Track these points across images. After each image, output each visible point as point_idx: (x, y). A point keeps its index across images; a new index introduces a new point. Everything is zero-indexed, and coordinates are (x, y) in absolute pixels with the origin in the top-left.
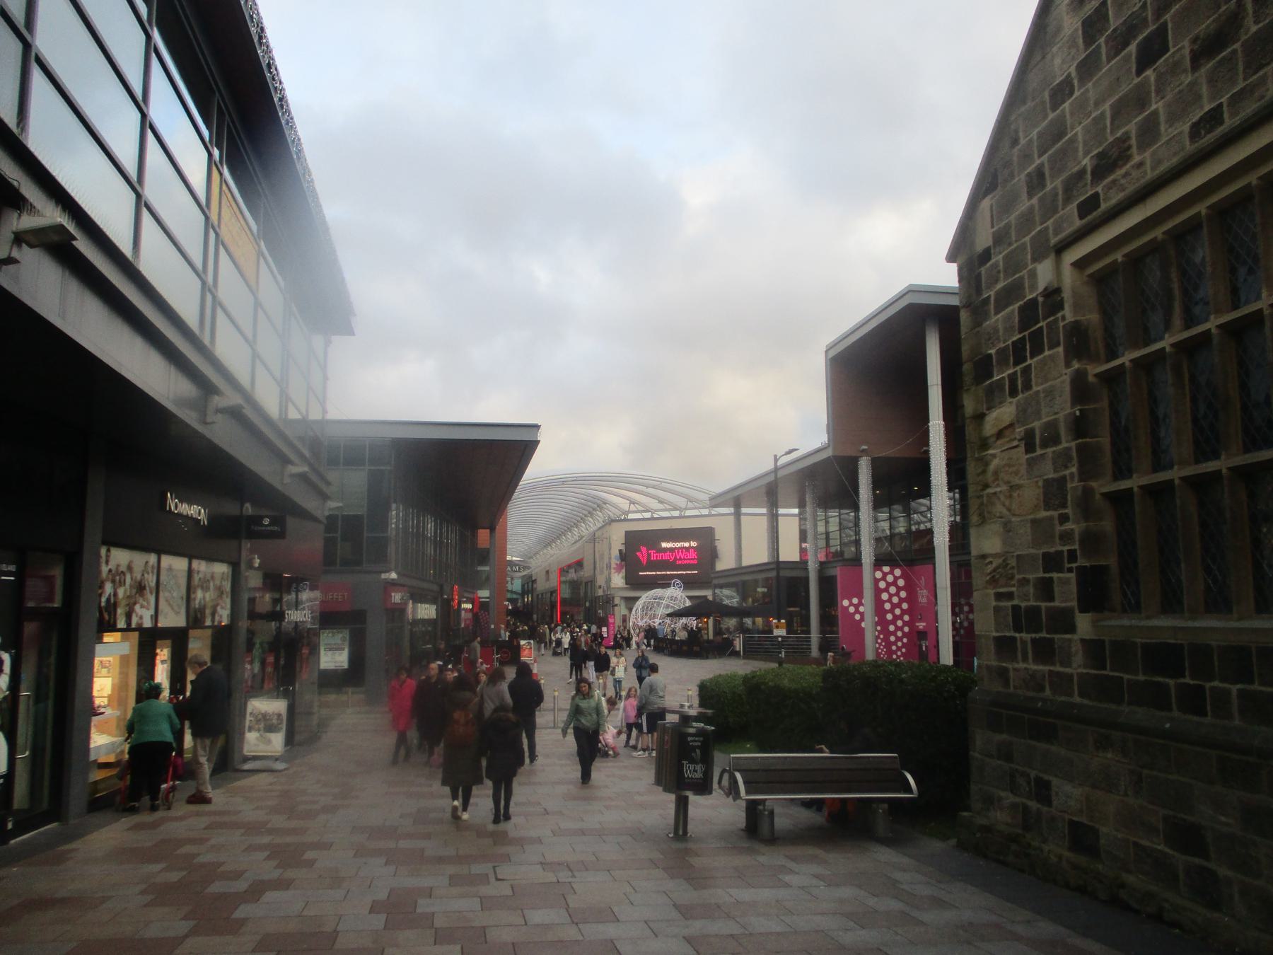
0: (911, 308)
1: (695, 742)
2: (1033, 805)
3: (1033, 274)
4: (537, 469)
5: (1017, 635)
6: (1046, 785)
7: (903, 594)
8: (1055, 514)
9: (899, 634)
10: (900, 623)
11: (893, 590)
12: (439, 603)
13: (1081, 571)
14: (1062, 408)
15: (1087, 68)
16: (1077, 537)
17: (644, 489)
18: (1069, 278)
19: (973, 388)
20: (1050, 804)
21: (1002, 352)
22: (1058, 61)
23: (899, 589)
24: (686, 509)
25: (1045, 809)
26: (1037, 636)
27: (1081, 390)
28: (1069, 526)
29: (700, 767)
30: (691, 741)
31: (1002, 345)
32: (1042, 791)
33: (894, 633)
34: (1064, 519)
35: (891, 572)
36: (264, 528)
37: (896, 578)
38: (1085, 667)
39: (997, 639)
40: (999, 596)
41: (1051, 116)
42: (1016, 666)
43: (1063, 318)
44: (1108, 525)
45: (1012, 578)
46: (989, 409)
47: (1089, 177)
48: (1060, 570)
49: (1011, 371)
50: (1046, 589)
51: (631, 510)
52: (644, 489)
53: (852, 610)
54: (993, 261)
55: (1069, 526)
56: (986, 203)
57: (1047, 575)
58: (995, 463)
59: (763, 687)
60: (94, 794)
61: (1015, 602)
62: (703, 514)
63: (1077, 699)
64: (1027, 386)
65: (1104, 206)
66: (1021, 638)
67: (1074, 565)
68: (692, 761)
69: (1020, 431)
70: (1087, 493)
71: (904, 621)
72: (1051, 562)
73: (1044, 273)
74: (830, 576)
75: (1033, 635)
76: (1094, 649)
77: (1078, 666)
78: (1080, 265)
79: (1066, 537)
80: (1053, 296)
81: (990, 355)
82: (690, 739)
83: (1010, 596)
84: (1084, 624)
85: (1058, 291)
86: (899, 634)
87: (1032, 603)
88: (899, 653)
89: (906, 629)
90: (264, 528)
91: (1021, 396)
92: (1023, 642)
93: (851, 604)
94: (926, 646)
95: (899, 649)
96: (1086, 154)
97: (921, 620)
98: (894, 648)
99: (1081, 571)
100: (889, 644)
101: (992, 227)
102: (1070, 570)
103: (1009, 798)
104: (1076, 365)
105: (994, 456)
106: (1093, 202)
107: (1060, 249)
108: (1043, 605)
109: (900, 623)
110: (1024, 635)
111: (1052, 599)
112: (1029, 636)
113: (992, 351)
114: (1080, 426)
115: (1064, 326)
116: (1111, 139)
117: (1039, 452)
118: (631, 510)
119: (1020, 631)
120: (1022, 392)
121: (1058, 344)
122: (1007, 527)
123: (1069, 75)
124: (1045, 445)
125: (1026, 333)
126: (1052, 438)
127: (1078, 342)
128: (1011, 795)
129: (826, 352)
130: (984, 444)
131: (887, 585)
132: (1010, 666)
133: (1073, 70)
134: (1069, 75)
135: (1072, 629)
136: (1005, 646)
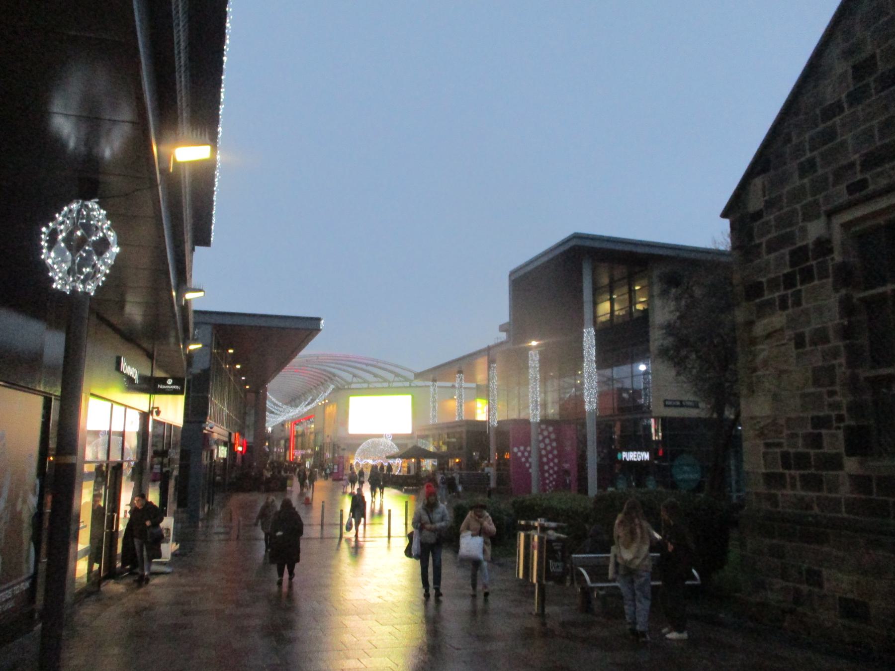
0: (573, 249)
1: (557, 546)
2: (805, 588)
3: (804, 230)
4: (312, 349)
5: (787, 472)
6: (819, 574)
7: (554, 444)
8: (824, 390)
9: (551, 472)
10: (551, 464)
11: (547, 441)
12: (228, 446)
13: (848, 428)
14: (833, 318)
15: (855, 98)
16: (845, 406)
17: (364, 367)
18: (837, 236)
19: (744, 304)
20: (821, 586)
21: (770, 281)
22: (829, 89)
23: (551, 441)
24: (393, 381)
25: (816, 590)
26: (806, 472)
27: (847, 308)
28: (837, 398)
29: (560, 564)
30: (555, 546)
31: (772, 276)
32: (814, 578)
33: (548, 471)
34: (832, 393)
35: (547, 429)
36: (168, 387)
37: (550, 433)
38: (852, 492)
39: (764, 474)
40: (767, 445)
41: (821, 126)
42: (785, 492)
43: (833, 259)
44: (868, 397)
45: (781, 433)
46: (759, 317)
47: (858, 168)
48: (830, 428)
49: (782, 292)
50: (815, 441)
51: (395, 380)
52: (364, 367)
53: (520, 454)
54: (764, 220)
55: (837, 398)
56: (758, 182)
57: (816, 431)
58: (761, 356)
59: (536, 508)
60: (583, 567)
61: (785, 449)
62: (359, 384)
63: (845, 515)
64: (798, 303)
65: (871, 187)
66: (790, 474)
67: (842, 425)
68: (556, 560)
69: (789, 333)
70: (854, 379)
71: (554, 463)
72: (820, 422)
73: (815, 229)
74: (182, 439)
75: (802, 472)
76: (861, 482)
77: (845, 492)
78: (846, 226)
79: (835, 406)
80: (823, 246)
81: (761, 283)
82: (554, 544)
83: (779, 445)
84: (851, 465)
85: (829, 241)
86: (551, 472)
87: (801, 449)
88: (551, 485)
89: (556, 469)
90: (168, 387)
91: (790, 311)
92: (793, 478)
93: (519, 451)
94: (570, 481)
95: (551, 482)
96: (856, 152)
97: (566, 462)
98: (547, 481)
99: (848, 428)
100: (544, 479)
101: (764, 196)
102: (839, 428)
103: (779, 583)
104: (843, 292)
105: (763, 350)
106: (863, 184)
107: (830, 214)
108: (812, 452)
109: (551, 464)
110: (793, 472)
111: (820, 446)
112: (798, 472)
113: (764, 280)
114: (846, 333)
115: (833, 265)
116: (878, 144)
117: (808, 348)
118: (395, 380)
119: (789, 468)
120: (793, 306)
121: (827, 277)
122: (776, 397)
123: (839, 101)
124: (814, 343)
125: (797, 268)
126: (821, 337)
127: (844, 277)
128: (781, 581)
129: (510, 276)
130: (753, 342)
131: (550, 441)
132: (779, 493)
133: (843, 96)
134: (839, 101)
135: (840, 466)
136: (772, 479)
